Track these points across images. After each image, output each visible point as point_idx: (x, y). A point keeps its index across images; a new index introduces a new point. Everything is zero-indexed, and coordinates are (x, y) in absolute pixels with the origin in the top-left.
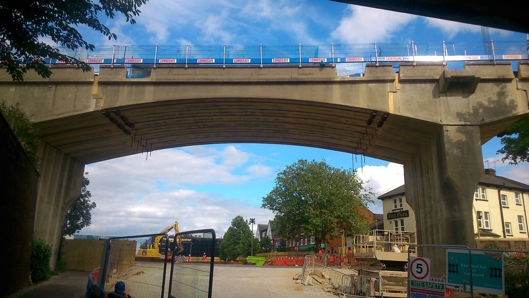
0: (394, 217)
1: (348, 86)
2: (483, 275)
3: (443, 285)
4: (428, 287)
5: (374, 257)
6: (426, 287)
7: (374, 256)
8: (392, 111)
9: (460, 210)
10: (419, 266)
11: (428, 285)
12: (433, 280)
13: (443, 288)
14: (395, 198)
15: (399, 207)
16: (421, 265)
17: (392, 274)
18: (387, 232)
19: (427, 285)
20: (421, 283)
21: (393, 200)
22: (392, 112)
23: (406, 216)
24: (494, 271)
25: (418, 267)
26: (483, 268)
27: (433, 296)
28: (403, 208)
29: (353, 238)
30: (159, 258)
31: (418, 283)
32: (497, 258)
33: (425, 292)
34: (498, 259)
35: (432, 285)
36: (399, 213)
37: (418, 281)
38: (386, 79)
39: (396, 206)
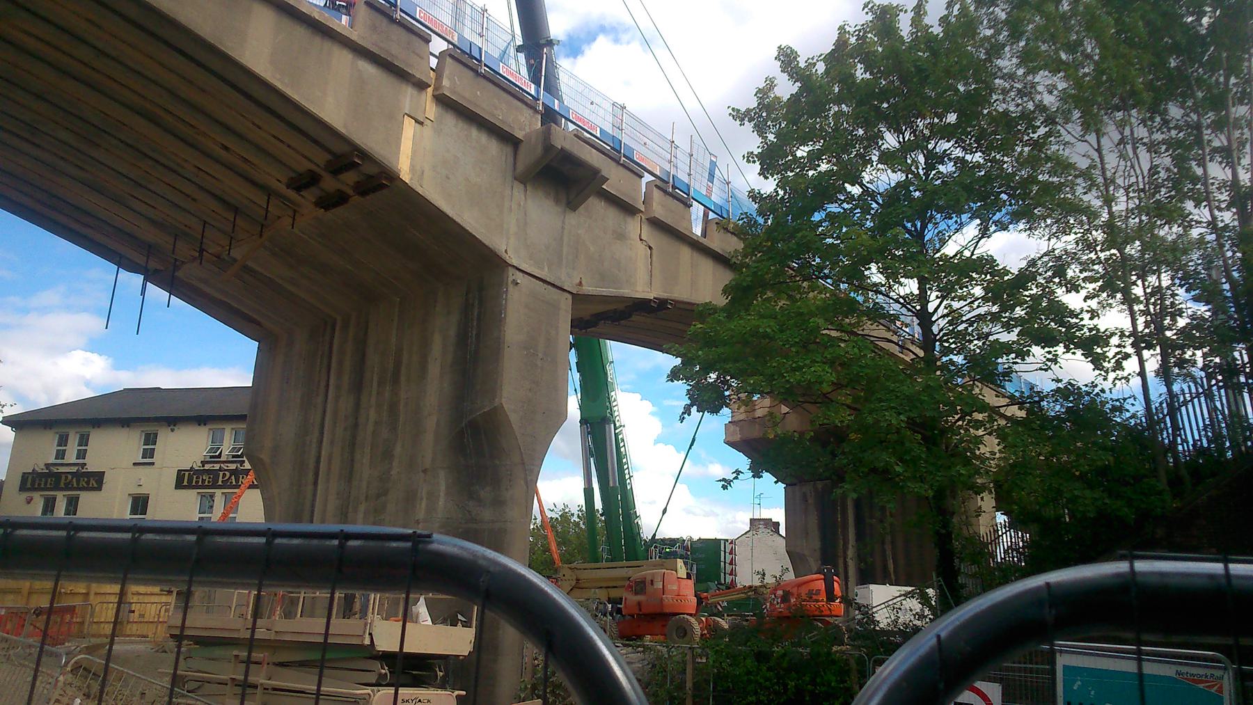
0: (48, 486)
1: (300, 31)
5: (367, 642)
7: (367, 636)
8: (404, 168)
9: (498, 503)
14: (63, 430)
15: (71, 457)
21: (78, 436)
22: (407, 177)
23: (93, 489)
28: (85, 464)
36: (70, 477)
38: (410, 72)
39: (61, 455)
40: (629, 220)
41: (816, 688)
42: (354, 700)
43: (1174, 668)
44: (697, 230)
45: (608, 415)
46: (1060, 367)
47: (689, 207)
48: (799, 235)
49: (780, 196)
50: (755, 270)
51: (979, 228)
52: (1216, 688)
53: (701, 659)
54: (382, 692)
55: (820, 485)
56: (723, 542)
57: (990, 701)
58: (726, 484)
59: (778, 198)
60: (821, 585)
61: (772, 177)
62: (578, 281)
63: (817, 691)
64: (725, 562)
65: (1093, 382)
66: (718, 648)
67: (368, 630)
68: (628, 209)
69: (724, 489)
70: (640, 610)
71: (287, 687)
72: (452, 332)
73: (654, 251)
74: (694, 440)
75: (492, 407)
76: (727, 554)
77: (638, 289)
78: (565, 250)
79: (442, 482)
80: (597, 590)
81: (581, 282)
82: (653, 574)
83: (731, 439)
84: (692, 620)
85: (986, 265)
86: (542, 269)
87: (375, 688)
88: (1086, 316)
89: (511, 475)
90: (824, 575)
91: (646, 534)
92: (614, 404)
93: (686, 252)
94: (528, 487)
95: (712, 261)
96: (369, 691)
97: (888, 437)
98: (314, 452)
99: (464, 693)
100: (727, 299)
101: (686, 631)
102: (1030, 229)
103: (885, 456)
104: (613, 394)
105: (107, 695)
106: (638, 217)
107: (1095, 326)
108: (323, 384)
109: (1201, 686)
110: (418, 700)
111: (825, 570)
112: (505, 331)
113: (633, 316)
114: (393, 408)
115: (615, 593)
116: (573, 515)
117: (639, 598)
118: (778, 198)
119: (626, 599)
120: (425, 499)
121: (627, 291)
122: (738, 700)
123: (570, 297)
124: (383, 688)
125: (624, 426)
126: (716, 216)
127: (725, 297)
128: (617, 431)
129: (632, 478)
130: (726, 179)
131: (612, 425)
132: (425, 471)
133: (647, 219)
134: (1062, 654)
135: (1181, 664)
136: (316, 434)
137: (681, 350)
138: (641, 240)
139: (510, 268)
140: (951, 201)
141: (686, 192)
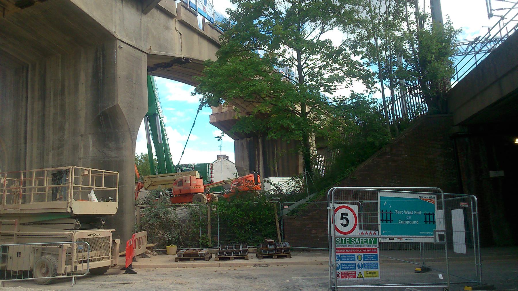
2: (418, 222)
3: (376, 238)
4: (357, 243)
5: (69, 210)
6: (355, 244)
9: (119, 149)
10: (344, 216)
11: (356, 242)
12: (362, 233)
13: (375, 243)
16: (347, 215)
17: (90, 235)
18: (87, 170)
19: (355, 242)
20: (347, 240)
24: (389, 218)
25: (342, 218)
26: (418, 213)
27: (363, 255)
29: (30, 178)
30: (8, 258)
31: (344, 240)
32: (430, 202)
33: (353, 250)
34: (431, 203)
35: (361, 240)
37: (344, 237)
40: (170, 20)
41: (261, 216)
42: (64, 237)
43: (419, 195)
44: (200, 27)
45: (157, 112)
46: (353, 87)
47: (197, 16)
48: (251, 29)
49: (239, 12)
50: (232, 44)
51: (320, 29)
52: (432, 202)
53: (214, 209)
54: (77, 232)
55: (248, 139)
56: (208, 164)
57: (354, 212)
58: (219, 139)
59: (238, 13)
60: (253, 178)
61: (236, 3)
62: (149, 48)
63: (261, 218)
64: (209, 173)
65: (362, 93)
66: (221, 204)
67: (69, 205)
68: (170, 15)
69: (219, 141)
70: (181, 193)
71: (30, 233)
72: (90, 71)
73: (182, 36)
74: (194, 123)
75: (113, 105)
76: (210, 169)
77: (176, 53)
78: (143, 32)
79: (90, 140)
80: (161, 186)
81: (150, 48)
82: (186, 178)
83: (212, 121)
84: (203, 195)
85: (326, 44)
86: (133, 41)
87: (74, 231)
88: (365, 66)
89: (124, 136)
90: (254, 174)
91: (175, 163)
92: (159, 107)
93: (196, 37)
94: (132, 141)
95: (207, 42)
96: (72, 232)
97: (288, 115)
98: (23, 129)
99: (115, 230)
100: (218, 57)
101: (201, 199)
102: (344, 29)
103: (287, 122)
104: (158, 103)
105: (117, 208)
106: (174, 20)
107: (369, 70)
108: (24, 96)
109: (427, 201)
110: (94, 235)
111: (254, 172)
112: (117, 70)
113: (173, 66)
114: (63, 106)
115: (169, 186)
116: (139, 157)
117: (179, 188)
118: (238, 13)
119: (174, 188)
120: (82, 148)
121: (171, 53)
122: (230, 224)
123: (146, 55)
124: (78, 230)
125: (164, 117)
126: (209, 21)
127: (217, 57)
128: (161, 119)
129: (168, 140)
130: (212, 4)
131: (159, 117)
132: (82, 136)
133: (178, 21)
134: (380, 192)
135: (421, 193)
136: (23, 121)
137: (200, 79)
138: (176, 30)
139: (117, 40)
140: (315, 13)
141: (195, 9)
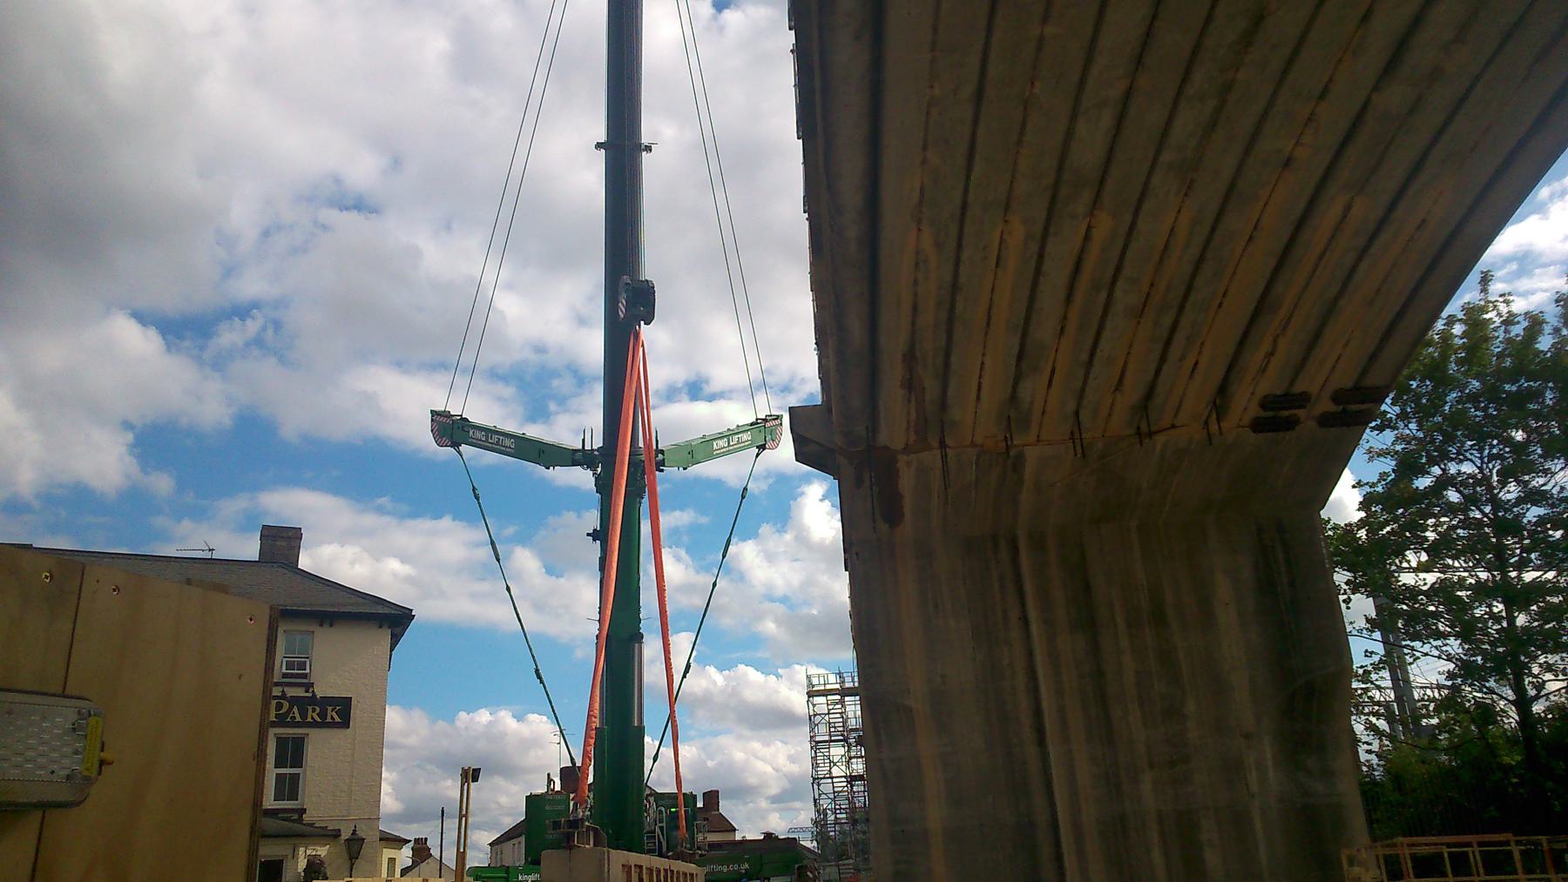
23: (333, 725)
108: (1014, 615)
